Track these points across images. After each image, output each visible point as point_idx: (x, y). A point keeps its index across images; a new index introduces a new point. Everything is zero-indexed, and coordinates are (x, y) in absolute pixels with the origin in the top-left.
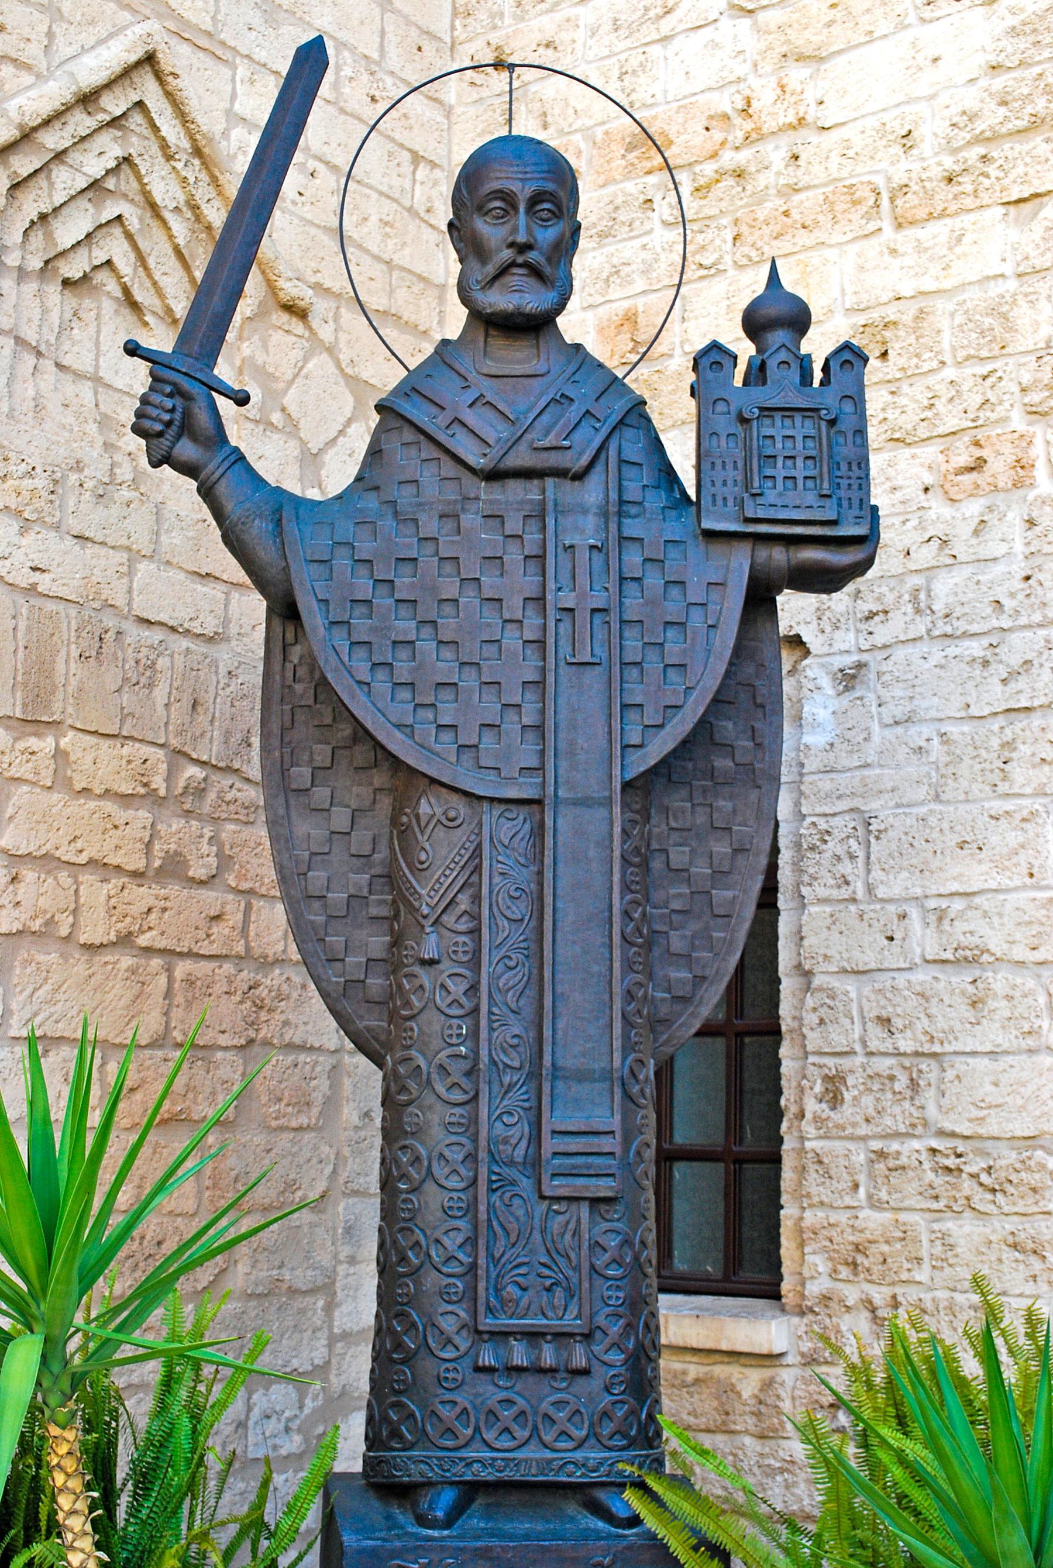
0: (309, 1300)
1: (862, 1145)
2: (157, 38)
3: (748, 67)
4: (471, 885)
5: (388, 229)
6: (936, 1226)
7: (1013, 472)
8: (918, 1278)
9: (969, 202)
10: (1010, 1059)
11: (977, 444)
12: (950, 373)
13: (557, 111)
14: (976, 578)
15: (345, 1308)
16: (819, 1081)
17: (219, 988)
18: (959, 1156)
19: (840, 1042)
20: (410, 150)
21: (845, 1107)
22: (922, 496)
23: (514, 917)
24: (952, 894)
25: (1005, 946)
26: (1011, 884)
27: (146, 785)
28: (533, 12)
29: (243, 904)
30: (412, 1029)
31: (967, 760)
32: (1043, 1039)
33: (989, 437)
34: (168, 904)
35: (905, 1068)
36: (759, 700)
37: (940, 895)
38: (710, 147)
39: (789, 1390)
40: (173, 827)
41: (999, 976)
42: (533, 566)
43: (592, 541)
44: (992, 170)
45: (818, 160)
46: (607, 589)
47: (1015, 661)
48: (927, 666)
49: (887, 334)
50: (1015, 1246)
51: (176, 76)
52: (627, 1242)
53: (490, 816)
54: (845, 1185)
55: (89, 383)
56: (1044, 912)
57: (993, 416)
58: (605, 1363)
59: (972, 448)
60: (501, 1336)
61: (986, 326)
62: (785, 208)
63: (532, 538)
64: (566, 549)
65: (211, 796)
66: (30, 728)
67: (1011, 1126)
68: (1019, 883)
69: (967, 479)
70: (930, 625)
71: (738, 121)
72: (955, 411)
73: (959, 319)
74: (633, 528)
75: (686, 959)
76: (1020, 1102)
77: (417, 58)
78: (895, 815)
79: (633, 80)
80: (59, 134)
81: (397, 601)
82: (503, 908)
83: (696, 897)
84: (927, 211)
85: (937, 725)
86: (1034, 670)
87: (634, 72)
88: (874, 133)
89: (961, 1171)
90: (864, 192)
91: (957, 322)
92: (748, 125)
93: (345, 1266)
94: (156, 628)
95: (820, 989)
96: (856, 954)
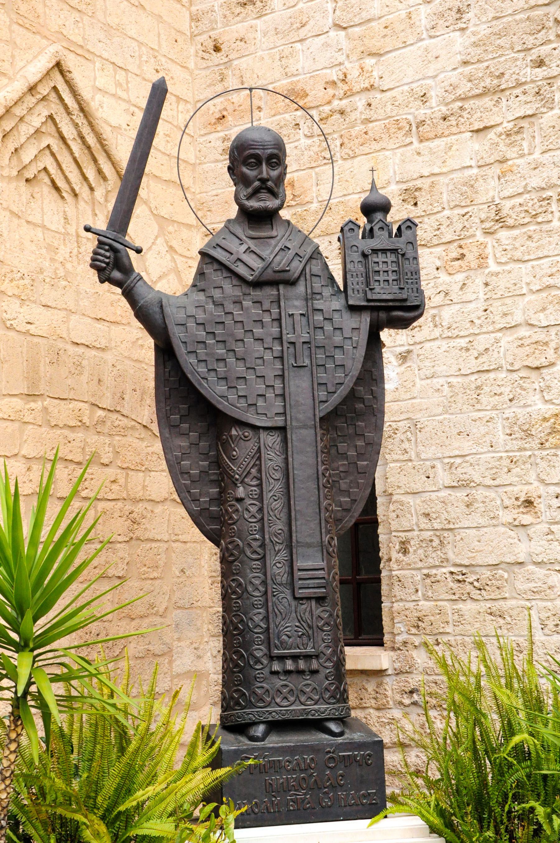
0: (161, 659)
1: (418, 572)
2: (60, 53)
3: (344, 57)
4: (256, 465)
5: (168, 138)
6: (455, 607)
7: (478, 260)
8: (447, 631)
9: (454, 130)
10: (485, 530)
11: (461, 247)
12: (447, 213)
13: (248, 76)
14: (462, 310)
15: (178, 662)
16: (398, 544)
17: (116, 515)
18: (463, 575)
19: (406, 525)
20: (175, 95)
21: (410, 555)
22: (436, 272)
23: (276, 478)
24: (456, 456)
25: (481, 479)
26: (482, 450)
27: (80, 421)
28: (233, 21)
29: (124, 474)
30: (234, 529)
31: (461, 395)
32: (500, 520)
33: (466, 244)
34: (93, 476)
35: (437, 536)
36: (374, 377)
37: (450, 457)
38: (327, 98)
39: (390, 686)
40: (92, 439)
41: (479, 492)
42: (276, 324)
43: (301, 312)
44: (465, 114)
45: (381, 107)
46: (308, 333)
47: (481, 348)
48: (440, 351)
49: (417, 194)
50: (491, 614)
51: (70, 72)
52: (331, 615)
53: (263, 435)
54: (413, 590)
55: (40, 229)
56: (498, 463)
57: (468, 234)
58: (325, 667)
59: (458, 249)
60: (282, 658)
61: (464, 191)
62: (365, 130)
63: (275, 311)
64: (290, 315)
65: (109, 424)
66: (31, 398)
67: (487, 560)
68: (486, 450)
69: (457, 263)
70: (441, 333)
71: (340, 84)
72: (450, 232)
73: (451, 187)
74: (318, 304)
75: (347, 493)
76: (491, 549)
77: (175, 46)
78: (428, 421)
79: (286, 61)
80: (21, 107)
81: (217, 341)
82: (271, 474)
83: (351, 465)
84: (434, 134)
85: (446, 379)
86: (489, 353)
87: (287, 56)
88: (408, 94)
89: (465, 581)
90: (403, 124)
91: (450, 189)
92: (346, 88)
93: (176, 642)
94: (80, 346)
95: (396, 502)
96: (412, 485)
